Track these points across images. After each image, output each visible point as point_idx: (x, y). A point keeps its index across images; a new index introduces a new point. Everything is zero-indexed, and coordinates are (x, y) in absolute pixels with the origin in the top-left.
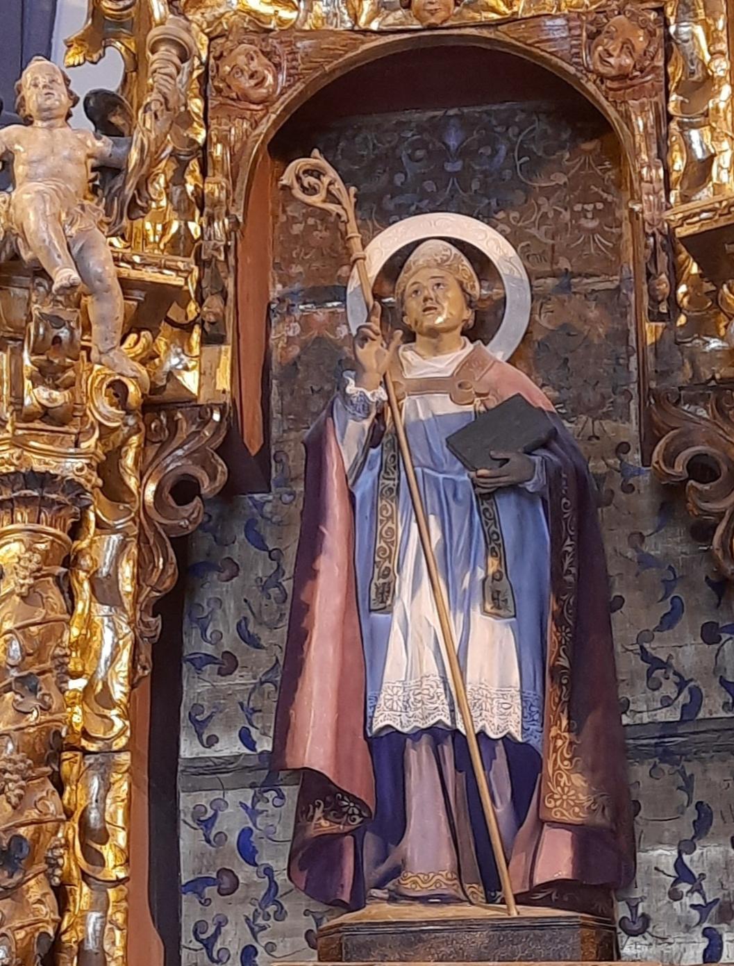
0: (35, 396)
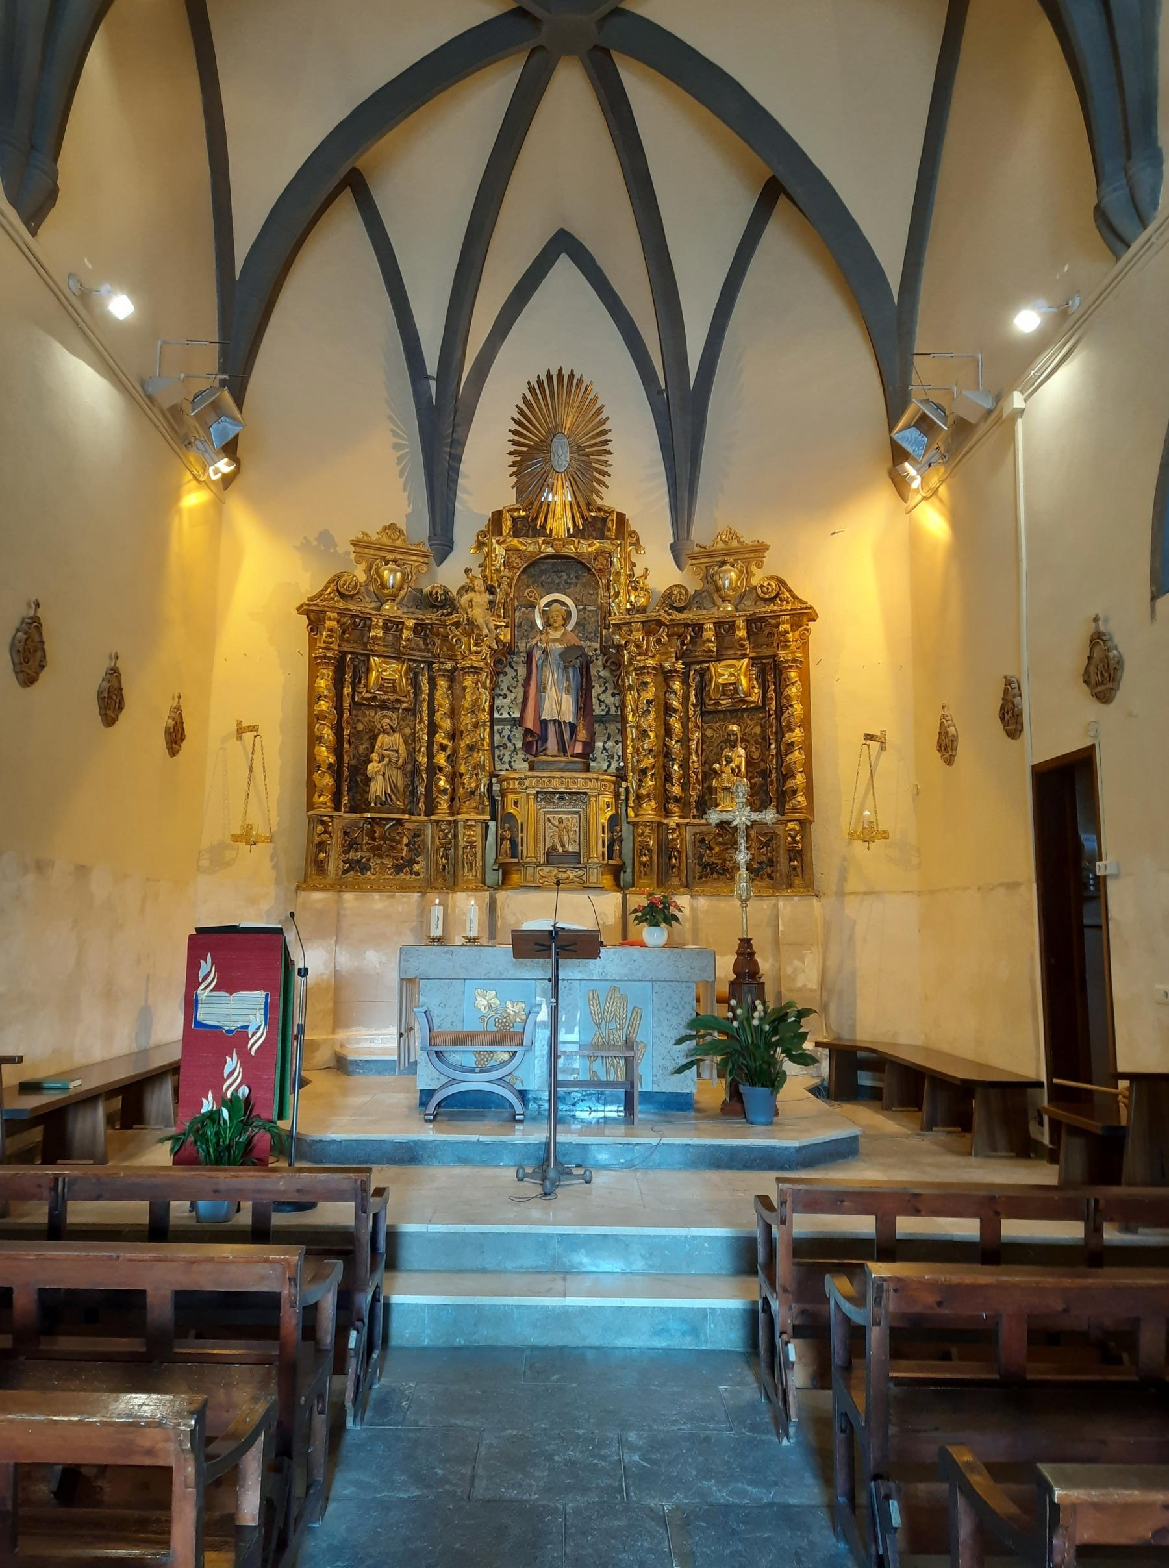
0: (474, 649)
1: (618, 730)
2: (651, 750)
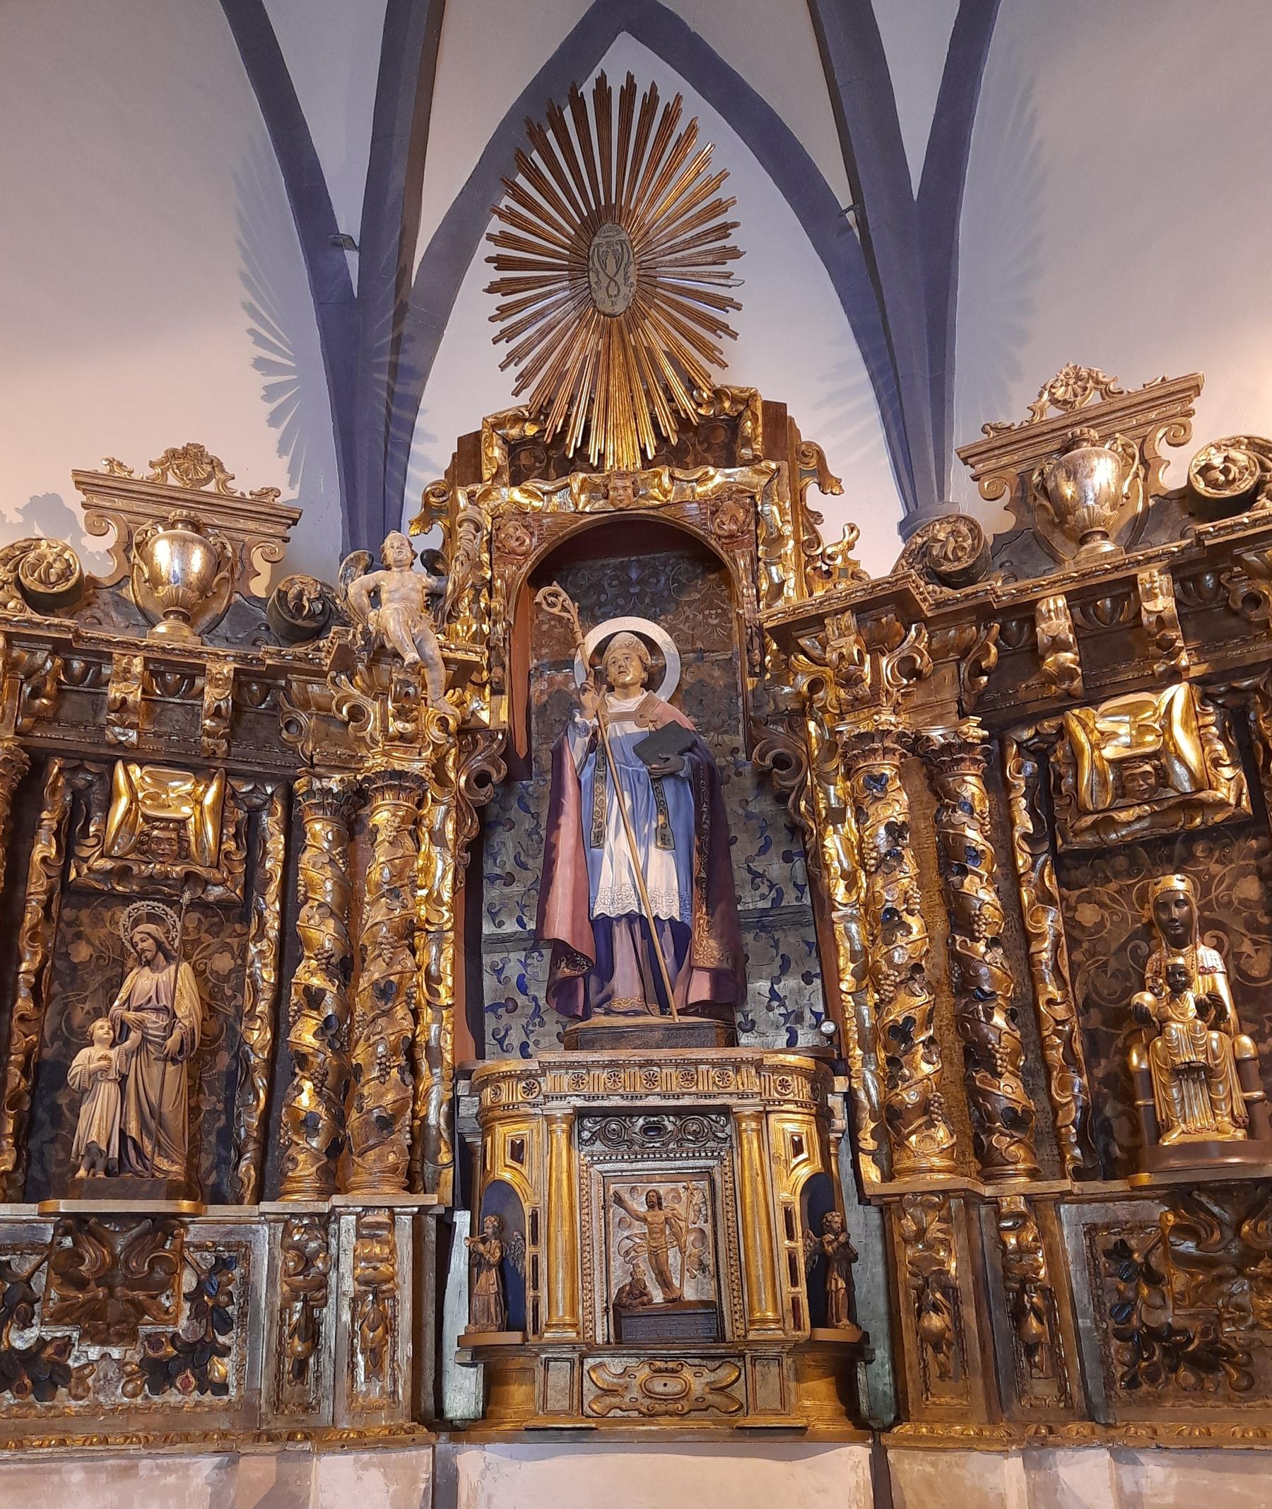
0: (396, 726)
1: (807, 943)
2: (917, 968)
